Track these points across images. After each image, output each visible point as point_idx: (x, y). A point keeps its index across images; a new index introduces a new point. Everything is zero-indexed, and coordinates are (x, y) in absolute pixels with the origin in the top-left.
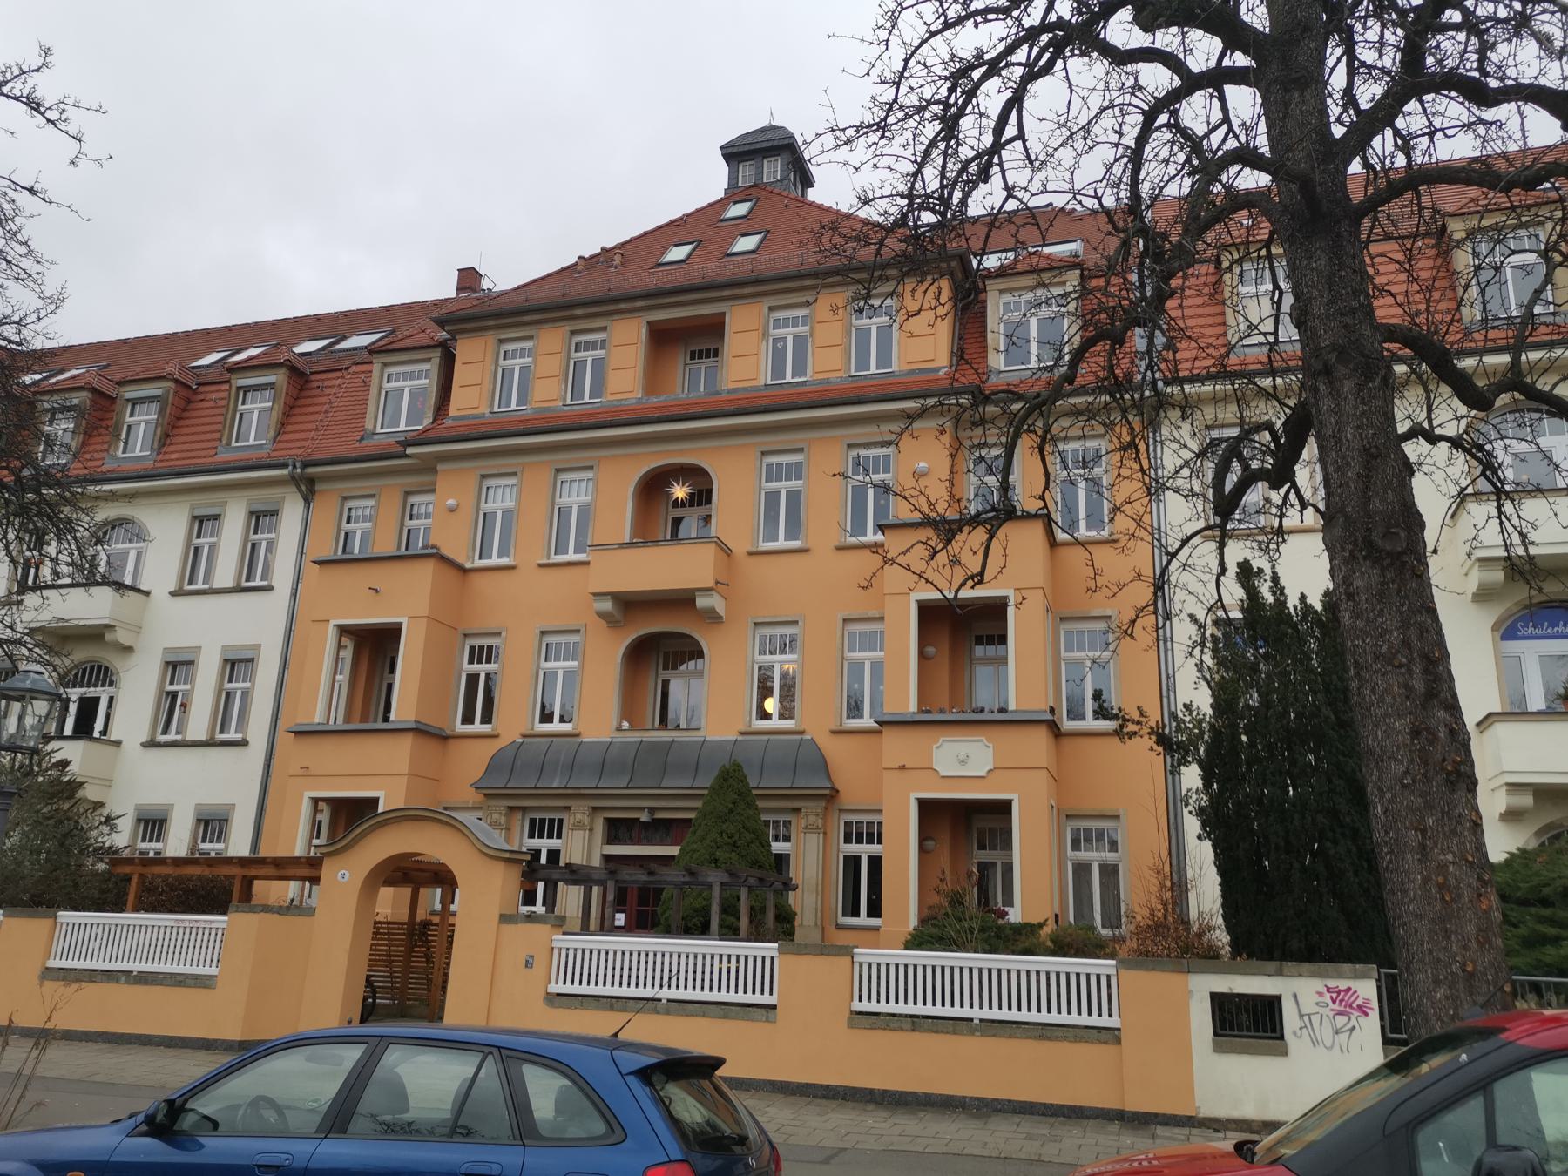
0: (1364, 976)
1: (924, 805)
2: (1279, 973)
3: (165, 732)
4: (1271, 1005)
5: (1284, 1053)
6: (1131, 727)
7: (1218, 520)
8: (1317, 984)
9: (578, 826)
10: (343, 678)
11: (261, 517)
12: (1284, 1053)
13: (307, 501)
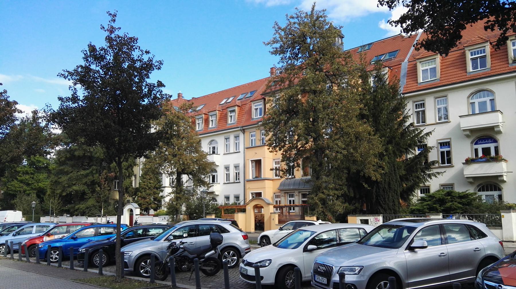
0: (379, 216)
4: (368, 220)
7: (90, 183)
8: (373, 217)
9: (296, 195)
10: (254, 169)
11: (237, 137)
13: (244, 134)
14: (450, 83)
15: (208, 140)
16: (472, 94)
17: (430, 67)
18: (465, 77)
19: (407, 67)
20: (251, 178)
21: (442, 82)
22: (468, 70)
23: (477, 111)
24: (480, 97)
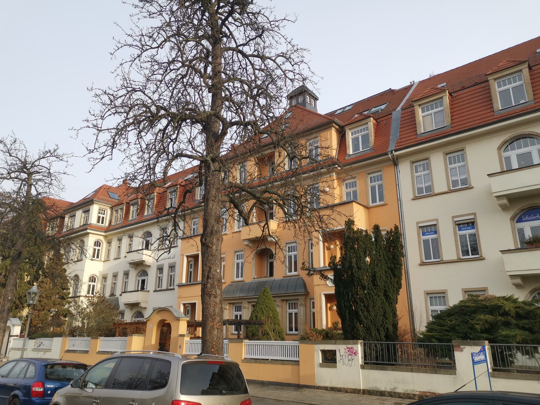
1: (195, 304)
2: (335, 344)
3: (159, 287)
4: (334, 353)
5: (336, 367)
6: (312, 272)
8: (344, 346)
9: (301, 305)
12: (336, 367)
14: (403, 146)
15: (140, 233)
16: (505, 142)
17: (513, 85)
18: (492, 118)
19: (400, 116)
20: (184, 281)
21: (455, 128)
22: (495, 108)
23: (515, 165)
24: (519, 147)
